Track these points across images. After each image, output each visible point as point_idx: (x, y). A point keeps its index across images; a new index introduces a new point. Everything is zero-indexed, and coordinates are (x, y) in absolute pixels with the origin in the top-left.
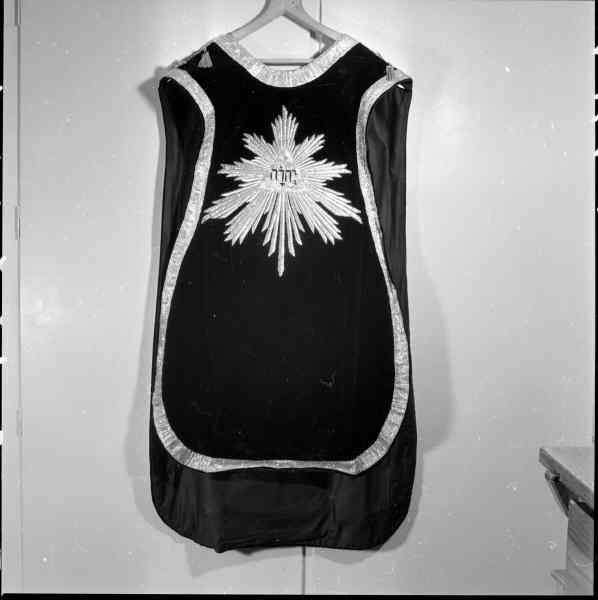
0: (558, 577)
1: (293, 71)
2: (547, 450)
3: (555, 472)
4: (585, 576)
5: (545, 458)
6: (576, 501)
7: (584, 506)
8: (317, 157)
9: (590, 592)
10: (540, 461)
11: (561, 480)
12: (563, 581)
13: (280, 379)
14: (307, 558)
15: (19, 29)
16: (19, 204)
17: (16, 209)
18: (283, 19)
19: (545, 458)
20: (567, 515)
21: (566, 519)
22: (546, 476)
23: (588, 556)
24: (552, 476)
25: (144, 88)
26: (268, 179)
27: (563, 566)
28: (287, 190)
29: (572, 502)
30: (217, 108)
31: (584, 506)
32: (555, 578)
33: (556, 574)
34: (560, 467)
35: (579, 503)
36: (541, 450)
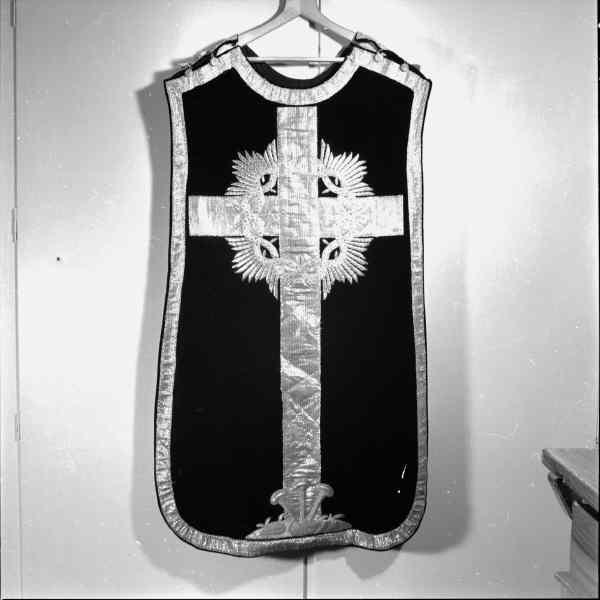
0: (563, 580)
1: (413, 173)
2: (550, 451)
3: (557, 474)
4: (592, 581)
5: (548, 460)
6: (580, 502)
7: (588, 508)
8: (270, 522)
9: (596, 596)
10: (544, 462)
11: (564, 481)
12: (567, 584)
13: (288, 400)
14: (309, 566)
15: (15, 31)
16: (16, 207)
17: (13, 212)
18: (300, 18)
19: (548, 460)
20: (571, 517)
21: (569, 522)
22: (550, 479)
23: (593, 559)
24: (555, 477)
25: (151, 100)
26: (284, 193)
27: (567, 568)
28: (302, 218)
29: (576, 504)
30: (223, 125)
31: (588, 508)
32: (559, 580)
33: (561, 576)
34: (561, 466)
35: (582, 505)
36: (544, 451)
